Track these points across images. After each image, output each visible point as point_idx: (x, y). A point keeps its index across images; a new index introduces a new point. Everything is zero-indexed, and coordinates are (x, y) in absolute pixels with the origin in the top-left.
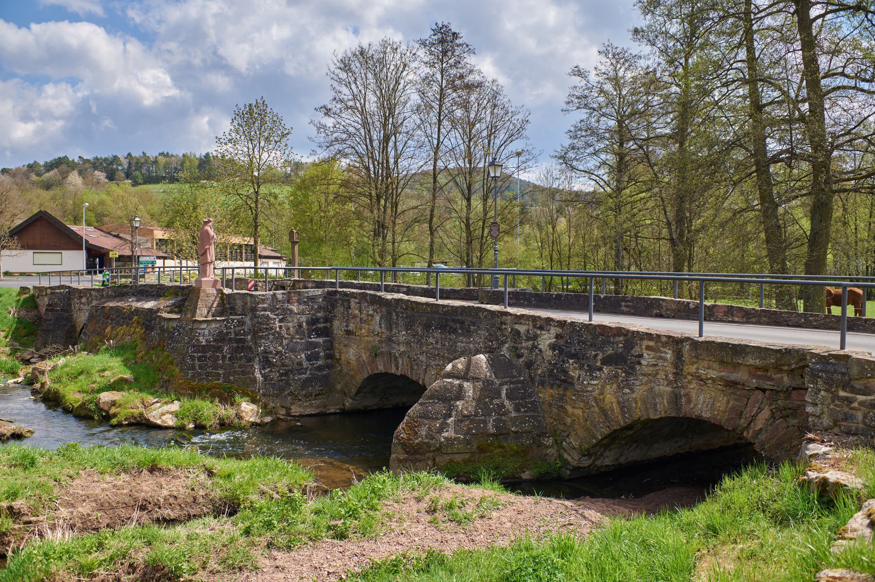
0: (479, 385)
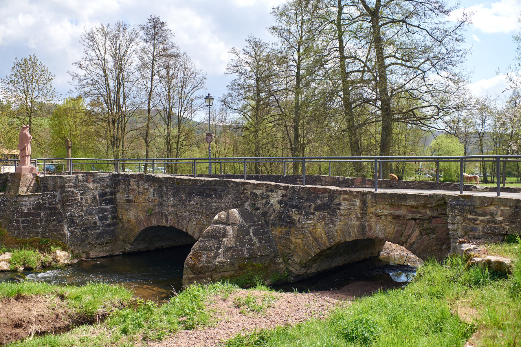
0: (236, 227)
